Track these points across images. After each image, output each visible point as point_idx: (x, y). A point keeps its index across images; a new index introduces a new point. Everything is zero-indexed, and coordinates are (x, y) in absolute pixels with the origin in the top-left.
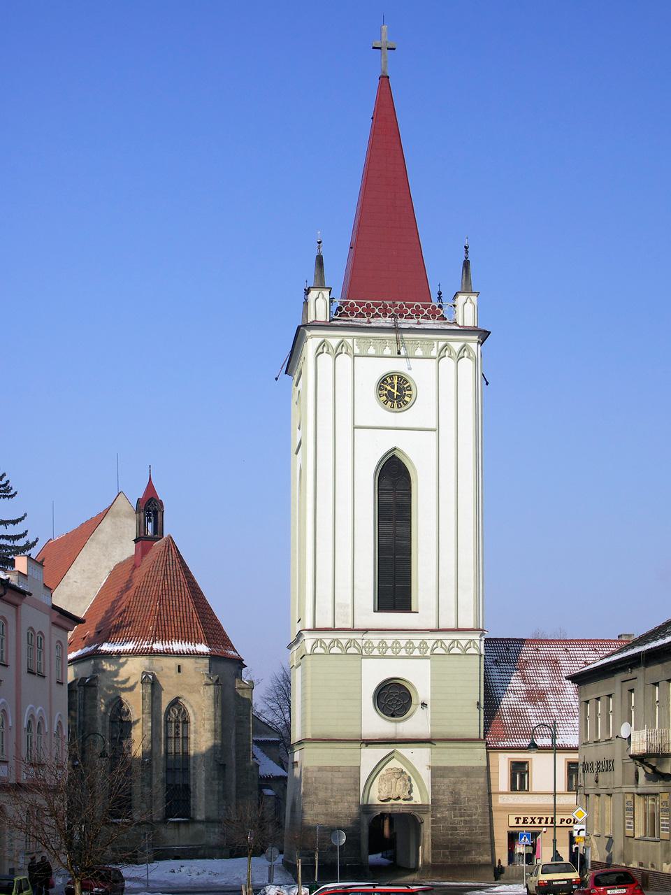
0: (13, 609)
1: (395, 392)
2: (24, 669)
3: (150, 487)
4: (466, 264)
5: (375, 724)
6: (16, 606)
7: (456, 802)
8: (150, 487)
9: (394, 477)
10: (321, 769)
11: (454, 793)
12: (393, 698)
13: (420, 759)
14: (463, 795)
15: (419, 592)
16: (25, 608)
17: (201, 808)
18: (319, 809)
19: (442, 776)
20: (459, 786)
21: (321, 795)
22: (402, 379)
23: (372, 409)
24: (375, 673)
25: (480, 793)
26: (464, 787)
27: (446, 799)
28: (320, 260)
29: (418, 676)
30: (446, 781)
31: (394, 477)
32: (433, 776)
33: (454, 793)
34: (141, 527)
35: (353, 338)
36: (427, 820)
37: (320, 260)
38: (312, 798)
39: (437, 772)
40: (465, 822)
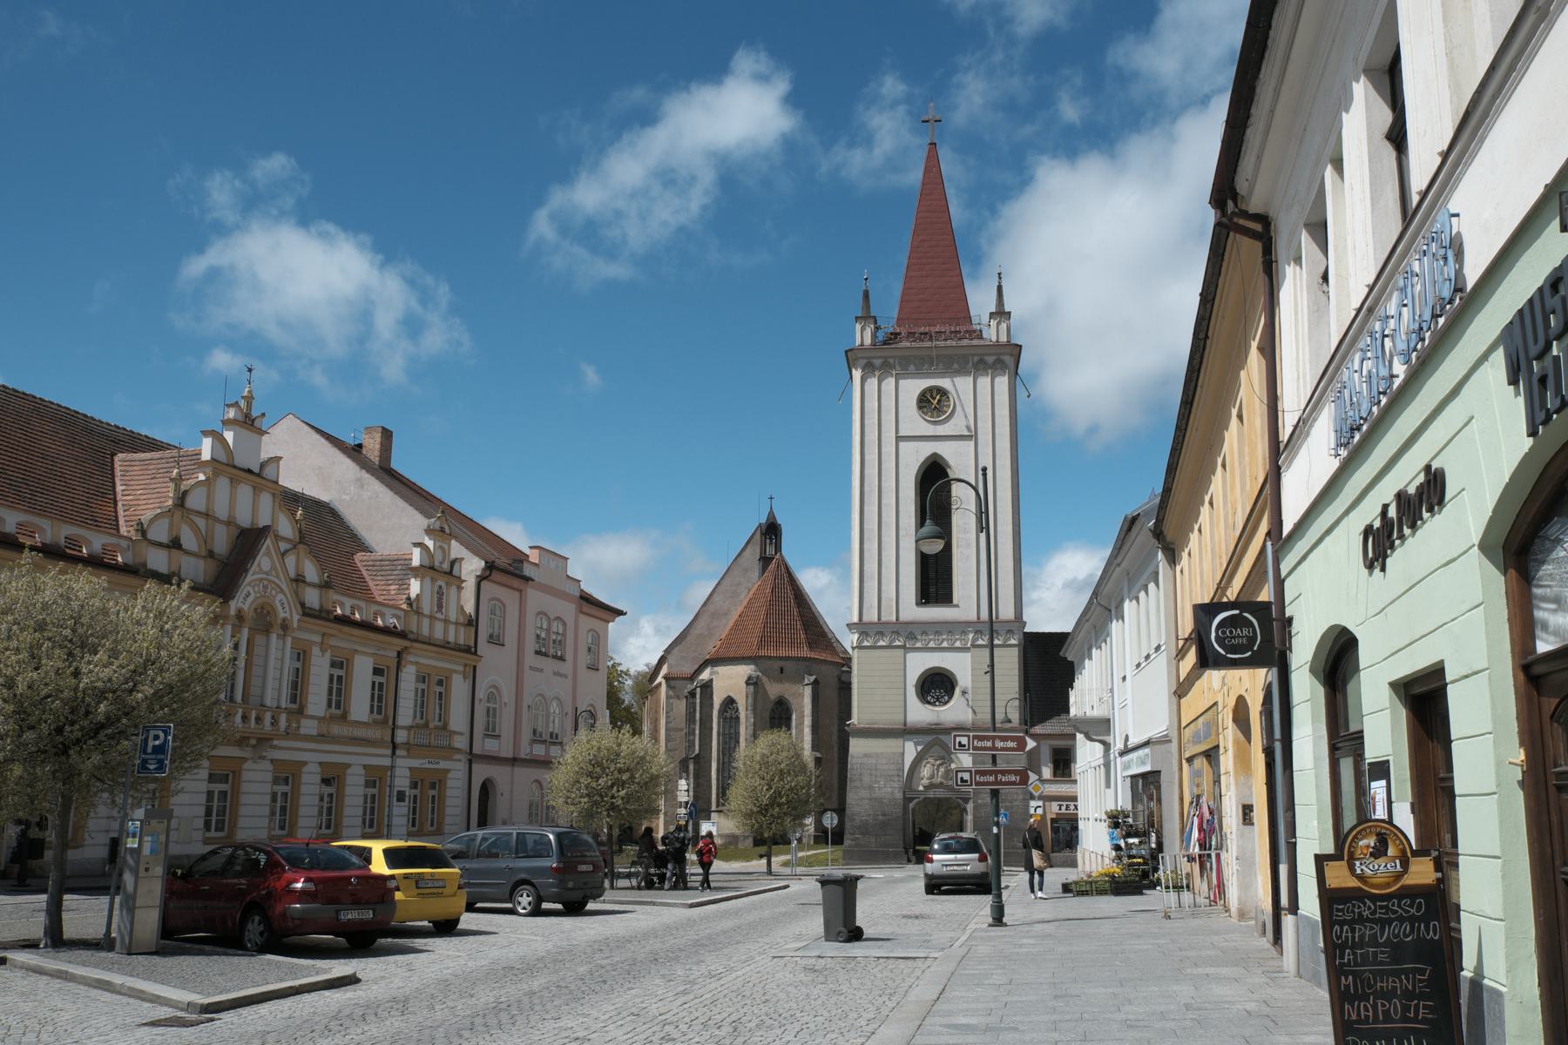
0: (517, 594)
1: (932, 403)
2: (530, 645)
3: (771, 515)
5: (920, 713)
8: (771, 515)
9: (934, 476)
10: (866, 755)
12: (937, 685)
17: (506, 700)
18: (864, 793)
21: (866, 780)
22: (943, 392)
23: (914, 422)
24: (919, 663)
28: (866, 295)
29: (962, 666)
31: (934, 476)
34: (763, 550)
36: (970, 806)
37: (866, 295)
38: (858, 784)
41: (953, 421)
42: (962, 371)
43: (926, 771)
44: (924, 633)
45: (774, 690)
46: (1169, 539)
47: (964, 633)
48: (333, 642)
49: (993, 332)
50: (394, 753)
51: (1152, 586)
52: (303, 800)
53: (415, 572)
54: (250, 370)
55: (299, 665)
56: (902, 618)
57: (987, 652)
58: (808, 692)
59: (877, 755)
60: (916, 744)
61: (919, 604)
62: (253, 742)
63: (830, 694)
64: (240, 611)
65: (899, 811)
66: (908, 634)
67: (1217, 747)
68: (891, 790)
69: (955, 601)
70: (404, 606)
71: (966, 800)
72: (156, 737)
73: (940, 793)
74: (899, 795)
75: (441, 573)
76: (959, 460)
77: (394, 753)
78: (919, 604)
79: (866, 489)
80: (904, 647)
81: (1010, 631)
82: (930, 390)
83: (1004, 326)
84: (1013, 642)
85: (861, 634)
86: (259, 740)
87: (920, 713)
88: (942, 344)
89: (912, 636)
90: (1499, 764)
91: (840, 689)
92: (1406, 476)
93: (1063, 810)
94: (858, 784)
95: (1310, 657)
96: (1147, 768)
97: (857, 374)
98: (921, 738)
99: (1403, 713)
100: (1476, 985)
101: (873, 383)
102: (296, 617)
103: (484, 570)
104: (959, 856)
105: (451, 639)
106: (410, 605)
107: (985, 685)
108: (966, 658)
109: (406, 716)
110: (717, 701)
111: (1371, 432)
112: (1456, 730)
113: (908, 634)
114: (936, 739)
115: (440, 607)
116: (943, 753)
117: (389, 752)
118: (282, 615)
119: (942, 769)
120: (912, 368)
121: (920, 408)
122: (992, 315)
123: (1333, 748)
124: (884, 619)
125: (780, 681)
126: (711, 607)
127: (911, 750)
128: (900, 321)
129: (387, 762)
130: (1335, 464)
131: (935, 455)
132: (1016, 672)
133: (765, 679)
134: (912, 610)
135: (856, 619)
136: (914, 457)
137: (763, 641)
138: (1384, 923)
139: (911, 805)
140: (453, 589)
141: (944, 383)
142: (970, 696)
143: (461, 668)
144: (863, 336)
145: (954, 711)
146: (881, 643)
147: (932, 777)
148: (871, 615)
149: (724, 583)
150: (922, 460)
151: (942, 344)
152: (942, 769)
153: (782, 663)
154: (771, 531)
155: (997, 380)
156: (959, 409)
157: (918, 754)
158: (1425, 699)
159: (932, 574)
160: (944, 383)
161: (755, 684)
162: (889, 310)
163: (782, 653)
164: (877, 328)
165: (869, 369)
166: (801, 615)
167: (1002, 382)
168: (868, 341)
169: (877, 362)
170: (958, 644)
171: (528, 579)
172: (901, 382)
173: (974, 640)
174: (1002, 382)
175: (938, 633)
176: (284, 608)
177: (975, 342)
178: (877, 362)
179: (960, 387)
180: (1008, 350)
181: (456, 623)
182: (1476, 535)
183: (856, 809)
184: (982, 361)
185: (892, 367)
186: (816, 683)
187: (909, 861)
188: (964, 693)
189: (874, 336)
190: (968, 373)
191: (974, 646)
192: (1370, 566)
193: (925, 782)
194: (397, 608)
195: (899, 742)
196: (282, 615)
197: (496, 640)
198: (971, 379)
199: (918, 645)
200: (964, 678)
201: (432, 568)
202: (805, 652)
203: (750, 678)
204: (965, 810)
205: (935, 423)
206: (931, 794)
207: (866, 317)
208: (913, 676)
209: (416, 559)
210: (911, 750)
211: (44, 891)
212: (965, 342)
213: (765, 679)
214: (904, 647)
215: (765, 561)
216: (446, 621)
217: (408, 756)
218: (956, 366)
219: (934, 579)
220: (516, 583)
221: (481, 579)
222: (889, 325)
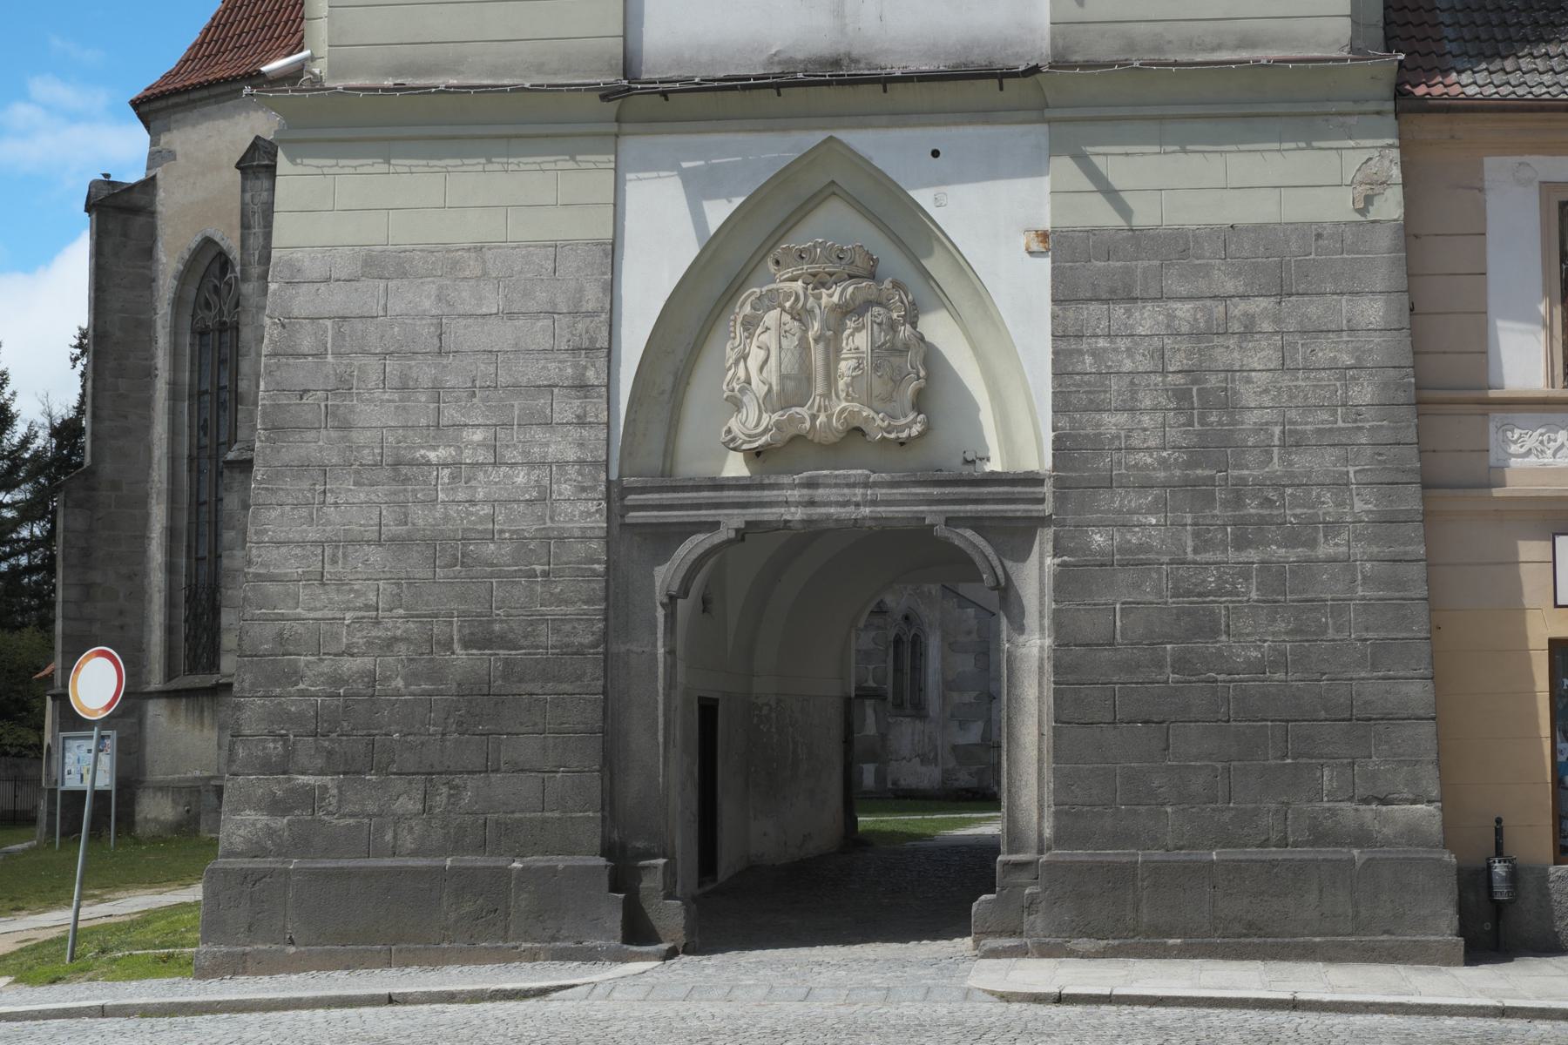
7: (1214, 447)
11: (1201, 398)
13: (995, 221)
14: (1258, 408)
18: (356, 507)
20: (1227, 354)
21: (375, 416)
25: (1364, 393)
26: (1260, 357)
27: (1145, 434)
30: (1147, 319)
33: (1201, 398)
36: (1034, 576)
38: (318, 445)
39: (1089, 271)
40: (1272, 575)
43: (754, 360)
57: (1347, 715)
59: (448, 263)
60: (698, 188)
65: (572, 612)
68: (528, 485)
71: (1015, 535)
73: (848, 497)
74: (582, 514)
94: (318, 445)
95: (945, 943)
110: (169, 260)
119: (858, 341)
127: (663, 224)
147: (794, 389)
152: (858, 341)
183: (308, 608)
187: (638, 932)
193: (751, 422)
204: (1006, 593)
206: (789, 505)
210: (663, 224)
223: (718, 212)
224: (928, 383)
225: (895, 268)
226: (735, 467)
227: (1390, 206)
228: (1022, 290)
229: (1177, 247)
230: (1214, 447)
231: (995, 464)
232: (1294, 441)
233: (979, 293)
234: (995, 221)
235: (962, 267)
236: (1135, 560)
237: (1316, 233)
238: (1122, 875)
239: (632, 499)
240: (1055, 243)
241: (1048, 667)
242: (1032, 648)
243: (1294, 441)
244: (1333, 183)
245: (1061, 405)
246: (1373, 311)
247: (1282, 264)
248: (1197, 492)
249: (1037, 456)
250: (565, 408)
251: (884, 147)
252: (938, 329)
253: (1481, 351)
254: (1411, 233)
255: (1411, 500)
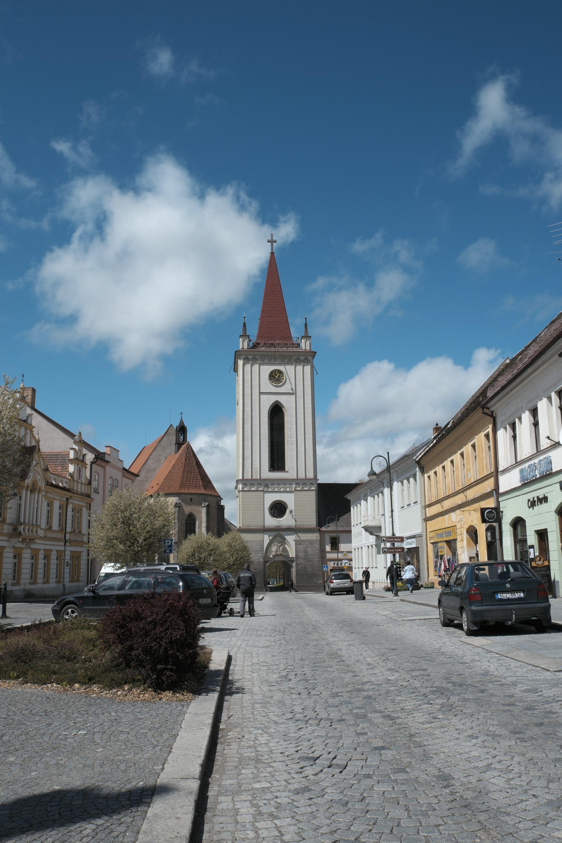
0: (102, 469)
4: (306, 325)
5: (271, 521)
6: (104, 467)
7: (307, 555)
9: (276, 412)
11: (306, 552)
12: (279, 509)
13: (291, 539)
14: (310, 553)
15: (198, 456)
16: (108, 468)
19: (300, 544)
20: (308, 549)
22: (280, 372)
23: (268, 386)
24: (270, 498)
25: (317, 552)
26: (310, 549)
27: (302, 555)
28: (245, 325)
29: (289, 499)
30: (302, 546)
31: (276, 412)
32: (296, 544)
33: (306, 552)
34: (177, 438)
35: (258, 355)
36: (294, 565)
37: (245, 325)
39: (298, 543)
40: (311, 565)
41: (285, 386)
42: (289, 363)
43: (274, 548)
44: (273, 484)
45: (188, 509)
46: (422, 464)
47: (291, 484)
48: (49, 495)
49: (305, 345)
50: (65, 545)
51: (412, 480)
52: (23, 566)
53: (71, 461)
54: (23, 376)
55: (49, 508)
56: (263, 477)
58: (204, 510)
60: (269, 536)
61: (270, 471)
62: (28, 541)
63: (214, 510)
64: (28, 484)
66: (265, 485)
67: (456, 539)
69: (286, 470)
70: (69, 477)
71: (292, 562)
72: (168, 542)
73: (281, 559)
74: (262, 560)
75: (79, 461)
76: (287, 402)
77: (65, 545)
78: (270, 471)
79: (245, 417)
80: (263, 491)
81: (311, 484)
82: (275, 371)
83: (308, 343)
84: (313, 488)
85: (243, 484)
86: (30, 539)
87: (271, 521)
88: (280, 350)
89: (267, 486)
90: (558, 546)
91: (218, 509)
92: (540, 494)
93: (336, 565)
96: (414, 546)
97: (240, 362)
98: (272, 533)
99: (537, 536)
100: (554, 581)
101: (248, 366)
102: (43, 485)
103: (94, 459)
104: (343, 580)
105: (79, 490)
106: (72, 477)
107: (302, 508)
108: (292, 496)
109: (69, 529)
111: (530, 482)
112: (549, 540)
113: (265, 485)
114: (279, 533)
115: (80, 477)
116: (281, 540)
117: (63, 544)
118: (40, 484)
119: (281, 548)
120: (266, 360)
121: (270, 379)
122: (302, 337)
123: (515, 542)
124: (254, 478)
125: (190, 505)
126: (147, 467)
127: (267, 539)
128: (259, 337)
129: (62, 548)
130: (520, 484)
131: (277, 401)
132: (315, 502)
133: (183, 504)
134: (267, 474)
135: (241, 478)
136: (267, 402)
137: (182, 486)
138: (541, 571)
139: (267, 564)
140: (84, 468)
141: (281, 368)
142: (293, 513)
143: (85, 505)
144: (243, 344)
145: (286, 521)
146: (253, 489)
147: (277, 551)
148: (248, 476)
149: (153, 454)
150: (271, 404)
151: (280, 350)
152: (281, 548)
153: (191, 496)
154: (182, 430)
155: (305, 367)
156: (288, 380)
157: (270, 540)
158: (542, 535)
159: (276, 457)
160: (281, 368)
161: (179, 507)
162: (253, 331)
163: (192, 491)
164: (250, 340)
165: (246, 360)
166: (200, 472)
167: (308, 368)
168: (246, 347)
169: (250, 357)
170: (288, 489)
171: (108, 462)
172: (261, 367)
173: (295, 488)
174: (308, 368)
175: (279, 484)
176: (41, 484)
177: (295, 349)
178: (250, 357)
179: (288, 370)
180: (310, 354)
181: (85, 484)
182: (554, 509)
184: (298, 359)
185: (258, 360)
186: (208, 506)
188: (291, 512)
189: (248, 345)
190: (292, 364)
191: (295, 490)
192: (529, 507)
193: (274, 553)
194: (65, 478)
195: (261, 535)
196: (40, 484)
197: (96, 492)
198: (294, 366)
199: (270, 490)
200: (291, 505)
201: (77, 459)
202: (202, 491)
203: (176, 504)
204: (292, 566)
205: (277, 386)
206: (276, 559)
207: (245, 335)
208: (267, 505)
209: (72, 455)
210: (267, 539)
211: (488, 559)
212: (290, 349)
213: (183, 504)
214: (263, 491)
215: (179, 445)
216: (82, 483)
217: (70, 546)
218: (286, 360)
219: (277, 460)
220: (103, 464)
221: (92, 463)
222: (254, 339)
223: (271, 538)
224: (285, 550)
225: (283, 541)
226: (271, 556)
227: (319, 538)
228: (293, 544)
229: (304, 541)
230: (307, 555)
231: (290, 556)
232: (312, 555)
233: (290, 544)
234: (291, 539)
235: (288, 542)
236: (301, 563)
237: (313, 540)
238: (301, 586)
239: (55, 526)
240: (295, 541)
241: (462, 509)
242: (294, 570)
243: (312, 555)
244: (315, 536)
245: (296, 552)
246: (318, 546)
247: (311, 542)
248: (305, 559)
249: (294, 556)
250: (260, 552)
251: (281, 533)
252: (286, 546)
253: (325, 548)
254: (320, 540)
255: (320, 559)
